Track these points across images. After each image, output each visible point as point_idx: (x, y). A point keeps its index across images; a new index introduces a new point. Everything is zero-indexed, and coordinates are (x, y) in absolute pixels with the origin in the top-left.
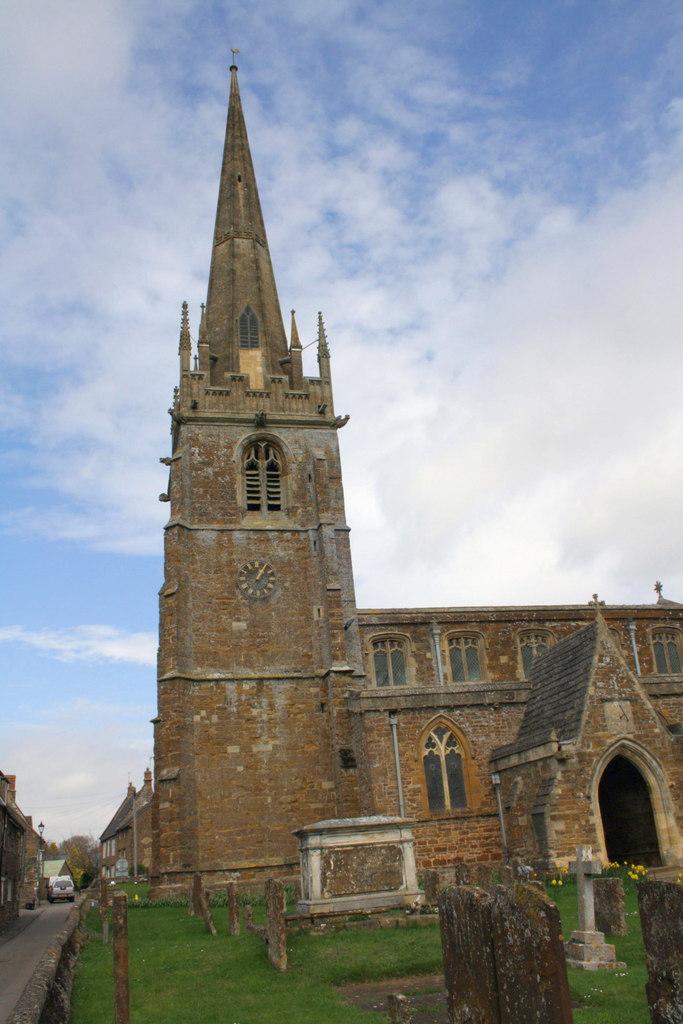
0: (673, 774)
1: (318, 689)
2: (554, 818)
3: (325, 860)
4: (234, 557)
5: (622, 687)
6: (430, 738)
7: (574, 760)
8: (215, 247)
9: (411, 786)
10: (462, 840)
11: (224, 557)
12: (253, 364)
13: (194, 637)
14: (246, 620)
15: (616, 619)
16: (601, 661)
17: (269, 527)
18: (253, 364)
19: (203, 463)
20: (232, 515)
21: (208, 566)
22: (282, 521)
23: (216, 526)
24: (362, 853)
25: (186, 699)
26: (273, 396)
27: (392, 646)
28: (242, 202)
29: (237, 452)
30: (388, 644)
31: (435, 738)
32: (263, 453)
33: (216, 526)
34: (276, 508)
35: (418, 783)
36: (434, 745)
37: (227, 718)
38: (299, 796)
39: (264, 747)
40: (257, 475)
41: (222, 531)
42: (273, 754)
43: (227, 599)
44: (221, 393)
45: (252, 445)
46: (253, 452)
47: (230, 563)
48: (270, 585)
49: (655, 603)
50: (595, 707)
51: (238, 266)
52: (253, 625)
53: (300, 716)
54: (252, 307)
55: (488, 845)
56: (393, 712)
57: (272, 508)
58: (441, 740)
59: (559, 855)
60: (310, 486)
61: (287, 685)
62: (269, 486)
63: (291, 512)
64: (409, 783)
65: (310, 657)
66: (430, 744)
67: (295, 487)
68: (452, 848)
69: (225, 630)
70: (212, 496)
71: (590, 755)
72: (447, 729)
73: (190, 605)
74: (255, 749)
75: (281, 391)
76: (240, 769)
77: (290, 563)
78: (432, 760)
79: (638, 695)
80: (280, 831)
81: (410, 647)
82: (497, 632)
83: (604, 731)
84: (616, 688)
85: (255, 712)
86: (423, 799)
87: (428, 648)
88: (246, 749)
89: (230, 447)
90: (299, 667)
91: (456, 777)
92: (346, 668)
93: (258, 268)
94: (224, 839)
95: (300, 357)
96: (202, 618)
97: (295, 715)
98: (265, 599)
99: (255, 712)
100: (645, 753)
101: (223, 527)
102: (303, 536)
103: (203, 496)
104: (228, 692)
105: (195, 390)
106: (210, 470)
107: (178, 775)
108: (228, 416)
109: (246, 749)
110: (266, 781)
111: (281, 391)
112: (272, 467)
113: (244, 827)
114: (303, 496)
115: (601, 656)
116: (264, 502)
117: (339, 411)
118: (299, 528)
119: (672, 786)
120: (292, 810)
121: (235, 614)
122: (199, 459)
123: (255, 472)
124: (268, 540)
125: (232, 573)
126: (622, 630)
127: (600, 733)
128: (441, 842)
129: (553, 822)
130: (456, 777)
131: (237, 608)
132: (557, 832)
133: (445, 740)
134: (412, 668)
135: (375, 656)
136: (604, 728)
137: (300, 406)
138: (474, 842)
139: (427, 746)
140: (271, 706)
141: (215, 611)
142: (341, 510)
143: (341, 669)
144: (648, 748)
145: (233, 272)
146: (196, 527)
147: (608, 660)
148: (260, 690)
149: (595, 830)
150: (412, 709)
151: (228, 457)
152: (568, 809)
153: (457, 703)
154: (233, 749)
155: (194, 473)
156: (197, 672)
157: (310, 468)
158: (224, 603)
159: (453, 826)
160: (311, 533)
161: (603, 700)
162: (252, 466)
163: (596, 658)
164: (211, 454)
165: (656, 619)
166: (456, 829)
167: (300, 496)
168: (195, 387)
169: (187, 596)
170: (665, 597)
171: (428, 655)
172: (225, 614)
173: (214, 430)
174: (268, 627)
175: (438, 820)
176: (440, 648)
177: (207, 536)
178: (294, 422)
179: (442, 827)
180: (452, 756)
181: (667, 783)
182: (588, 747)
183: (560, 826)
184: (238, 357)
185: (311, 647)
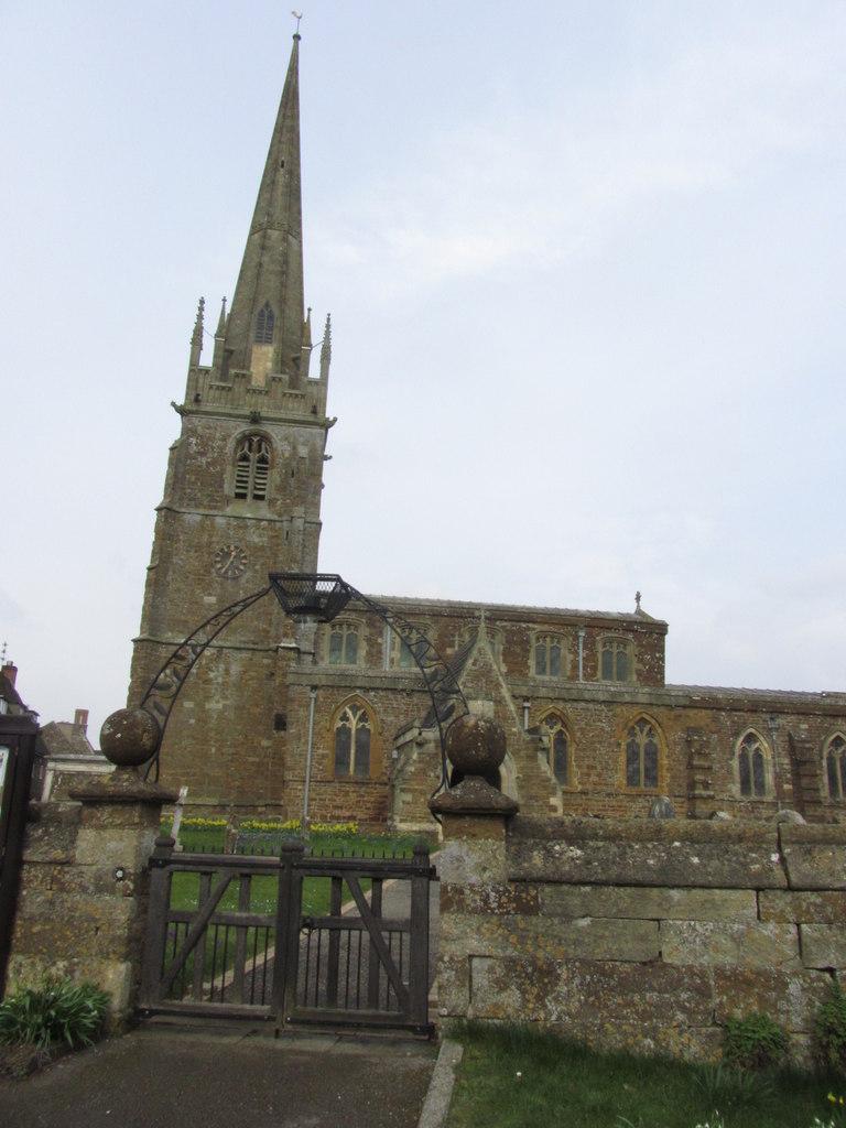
0: (522, 768)
1: (270, 661)
2: (402, 790)
3: (56, 777)
4: (214, 539)
6: (345, 713)
8: (251, 234)
9: (320, 751)
11: (205, 538)
12: (263, 360)
15: (567, 625)
16: (474, 664)
18: (263, 360)
20: (217, 502)
21: (190, 546)
22: (264, 511)
24: (81, 777)
27: (349, 629)
29: (231, 444)
30: (345, 626)
31: (350, 713)
32: (255, 447)
33: (202, 511)
34: (261, 498)
35: (326, 749)
36: (347, 719)
39: (215, 705)
42: (221, 713)
44: (223, 388)
45: (246, 438)
46: (247, 445)
47: (210, 544)
48: (242, 567)
49: (633, 612)
54: (271, 302)
56: (314, 688)
58: (354, 715)
59: (401, 821)
60: (292, 481)
61: (245, 655)
63: (272, 502)
64: (318, 748)
65: (268, 632)
66: (345, 718)
73: (169, 578)
74: (207, 706)
75: (280, 391)
76: (192, 721)
77: (262, 548)
78: (344, 731)
79: (504, 697)
81: (364, 631)
82: (448, 626)
85: (212, 675)
86: (329, 763)
87: (381, 634)
88: (201, 706)
90: (257, 640)
91: (363, 749)
92: (294, 645)
94: (170, 778)
95: (309, 355)
98: (235, 579)
99: (212, 675)
103: (194, 483)
105: (200, 385)
106: (204, 460)
108: (226, 411)
109: (201, 706)
110: (212, 734)
111: (280, 391)
112: (263, 460)
115: (476, 660)
117: (330, 414)
118: (276, 517)
120: (232, 761)
121: (207, 590)
124: (247, 527)
125: (210, 553)
128: (339, 801)
130: (363, 749)
131: (210, 585)
132: (403, 802)
133: (358, 717)
134: (362, 652)
135: (332, 636)
139: (342, 719)
140: (227, 671)
142: (317, 505)
143: (291, 646)
145: (260, 265)
146: (183, 510)
150: (332, 687)
151: (222, 449)
152: (417, 784)
154: (188, 705)
157: (294, 464)
159: (353, 789)
162: (245, 458)
163: (470, 661)
165: (609, 628)
167: (282, 488)
168: (201, 381)
170: (643, 609)
173: (211, 421)
175: (340, 782)
177: (192, 517)
178: (285, 421)
181: (514, 775)
183: (408, 797)
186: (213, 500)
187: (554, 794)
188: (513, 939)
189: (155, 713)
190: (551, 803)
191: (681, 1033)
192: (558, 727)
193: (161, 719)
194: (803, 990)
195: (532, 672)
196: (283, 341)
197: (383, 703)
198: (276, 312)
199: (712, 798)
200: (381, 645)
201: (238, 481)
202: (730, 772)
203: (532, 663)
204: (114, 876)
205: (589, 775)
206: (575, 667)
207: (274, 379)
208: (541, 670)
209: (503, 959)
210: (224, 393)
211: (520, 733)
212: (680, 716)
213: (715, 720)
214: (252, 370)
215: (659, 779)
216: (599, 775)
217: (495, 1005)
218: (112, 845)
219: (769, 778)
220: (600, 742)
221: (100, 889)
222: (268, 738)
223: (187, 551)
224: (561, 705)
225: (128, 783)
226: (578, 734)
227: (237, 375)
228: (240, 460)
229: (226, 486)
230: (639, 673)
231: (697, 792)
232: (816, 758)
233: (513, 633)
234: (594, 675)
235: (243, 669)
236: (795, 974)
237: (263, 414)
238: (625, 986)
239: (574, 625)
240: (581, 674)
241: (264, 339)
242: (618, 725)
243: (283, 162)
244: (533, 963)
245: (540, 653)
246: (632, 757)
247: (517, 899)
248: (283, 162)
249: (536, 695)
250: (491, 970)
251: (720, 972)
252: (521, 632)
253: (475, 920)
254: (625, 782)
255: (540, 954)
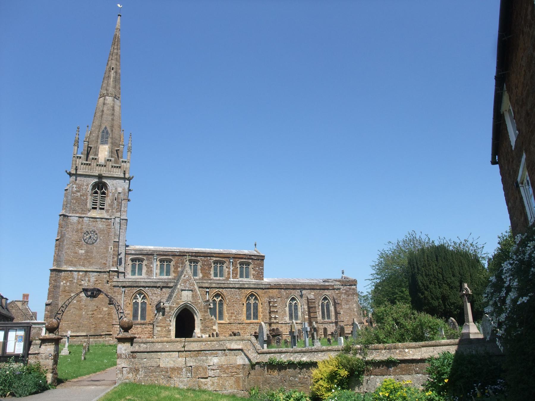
0: (202, 316)
2: (157, 326)
4: (83, 227)
5: (190, 286)
7: (168, 308)
10: (142, 331)
11: (80, 227)
13: (65, 255)
14: (84, 250)
16: (184, 277)
17: (98, 217)
19: (77, 191)
21: (73, 230)
22: (104, 215)
23: (78, 215)
25: (58, 276)
26: (107, 166)
28: (112, 79)
29: (90, 187)
34: (103, 209)
36: (137, 299)
37: (73, 284)
38: (94, 312)
40: (97, 196)
41: (80, 217)
43: (79, 242)
45: (95, 186)
47: (81, 229)
50: (178, 292)
51: (105, 109)
52: (87, 252)
53: (99, 285)
55: (151, 333)
57: (101, 209)
58: (140, 297)
61: (96, 274)
62: (101, 199)
63: (107, 211)
65: (106, 264)
67: (110, 202)
68: (138, 334)
69: (76, 253)
70: (78, 204)
71: (174, 307)
72: (143, 294)
73: (65, 243)
77: (103, 230)
78: (136, 303)
79: (196, 289)
80: (86, 324)
83: (180, 300)
84: (188, 286)
85: (83, 282)
87: (152, 263)
89: (87, 185)
92: (116, 269)
93: (113, 110)
96: (68, 248)
97: (97, 284)
100: (194, 308)
101: (80, 215)
102: (109, 221)
103: (75, 204)
104: (74, 275)
105: (77, 163)
106: (79, 194)
107: (51, 303)
110: (83, 307)
113: (74, 322)
114: (112, 205)
115: (185, 275)
116: (98, 206)
118: (108, 217)
119: (201, 320)
121: (80, 247)
122: (75, 189)
123: (97, 195)
124: (97, 221)
125: (81, 233)
126: (228, 261)
127: (179, 301)
129: (157, 328)
130: (144, 310)
135: (138, 264)
136: (181, 299)
137: (117, 170)
138: (146, 332)
140: (89, 281)
141: (74, 246)
144: (195, 307)
145: (103, 111)
146: (70, 215)
147: (187, 277)
148: (85, 275)
149: (171, 331)
151: (86, 189)
153: (147, 285)
155: (73, 195)
156: (64, 268)
157: (116, 195)
158: (77, 243)
160: (112, 219)
161: (182, 290)
163: (183, 276)
164: (80, 187)
166: (140, 327)
167: (111, 205)
168: (78, 161)
169: (64, 240)
171: (151, 266)
172: (77, 247)
174: (92, 253)
176: (156, 265)
177: (74, 219)
179: (136, 326)
180: (143, 303)
182: (174, 305)
183: (159, 329)
184: (99, 148)
185: (107, 260)
186: (82, 211)
187: (215, 325)
188: (131, 363)
189: (58, 320)
190: (214, 328)
191: (162, 380)
192: (220, 298)
193: (59, 321)
194: (186, 370)
195: (212, 276)
196: (112, 143)
197: (151, 292)
198: (110, 132)
199: (278, 323)
200: (152, 267)
201: (93, 202)
202: (285, 312)
203: (212, 272)
204: (49, 356)
205: (232, 316)
206: (229, 274)
207: (108, 160)
208: (216, 275)
209: (129, 368)
210: (87, 166)
211: (202, 302)
212: (266, 292)
213: (279, 292)
214: (99, 156)
215: (259, 316)
216: (235, 316)
217: (127, 377)
218: (49, 349)
219: (300, 314)
220: (236, 304)
221: (46, 359)
222: (106, 307)
223: (72, 232)
224: (221, 290)
225: (52, 336)
226: (228, 301)
227: (93, 159)
228: (94, 194)
229: (88, 205)
230: (254, 275)
231: (272, 321)
232: (317, 305)
233: (205, 261)
234: (236, 276)
235: (96, 280)
236: (184, 367)
237: (103, 175)
238: (152, 372)
239: (229, 258)
240: (231, 276)
241: (104, 142)
242: (243, 297)
243: (113, 68)
244: (135, 368)
245: (215, 269)
246: (248, 309)
247: (132, 356)
248: (113, 68)
249: (211, 286)
250: (127, 370)
251: (170, 368)
252: (208, 261)
253: (124, 360)
254: (246, 318)
255: (136, 366)
